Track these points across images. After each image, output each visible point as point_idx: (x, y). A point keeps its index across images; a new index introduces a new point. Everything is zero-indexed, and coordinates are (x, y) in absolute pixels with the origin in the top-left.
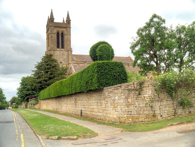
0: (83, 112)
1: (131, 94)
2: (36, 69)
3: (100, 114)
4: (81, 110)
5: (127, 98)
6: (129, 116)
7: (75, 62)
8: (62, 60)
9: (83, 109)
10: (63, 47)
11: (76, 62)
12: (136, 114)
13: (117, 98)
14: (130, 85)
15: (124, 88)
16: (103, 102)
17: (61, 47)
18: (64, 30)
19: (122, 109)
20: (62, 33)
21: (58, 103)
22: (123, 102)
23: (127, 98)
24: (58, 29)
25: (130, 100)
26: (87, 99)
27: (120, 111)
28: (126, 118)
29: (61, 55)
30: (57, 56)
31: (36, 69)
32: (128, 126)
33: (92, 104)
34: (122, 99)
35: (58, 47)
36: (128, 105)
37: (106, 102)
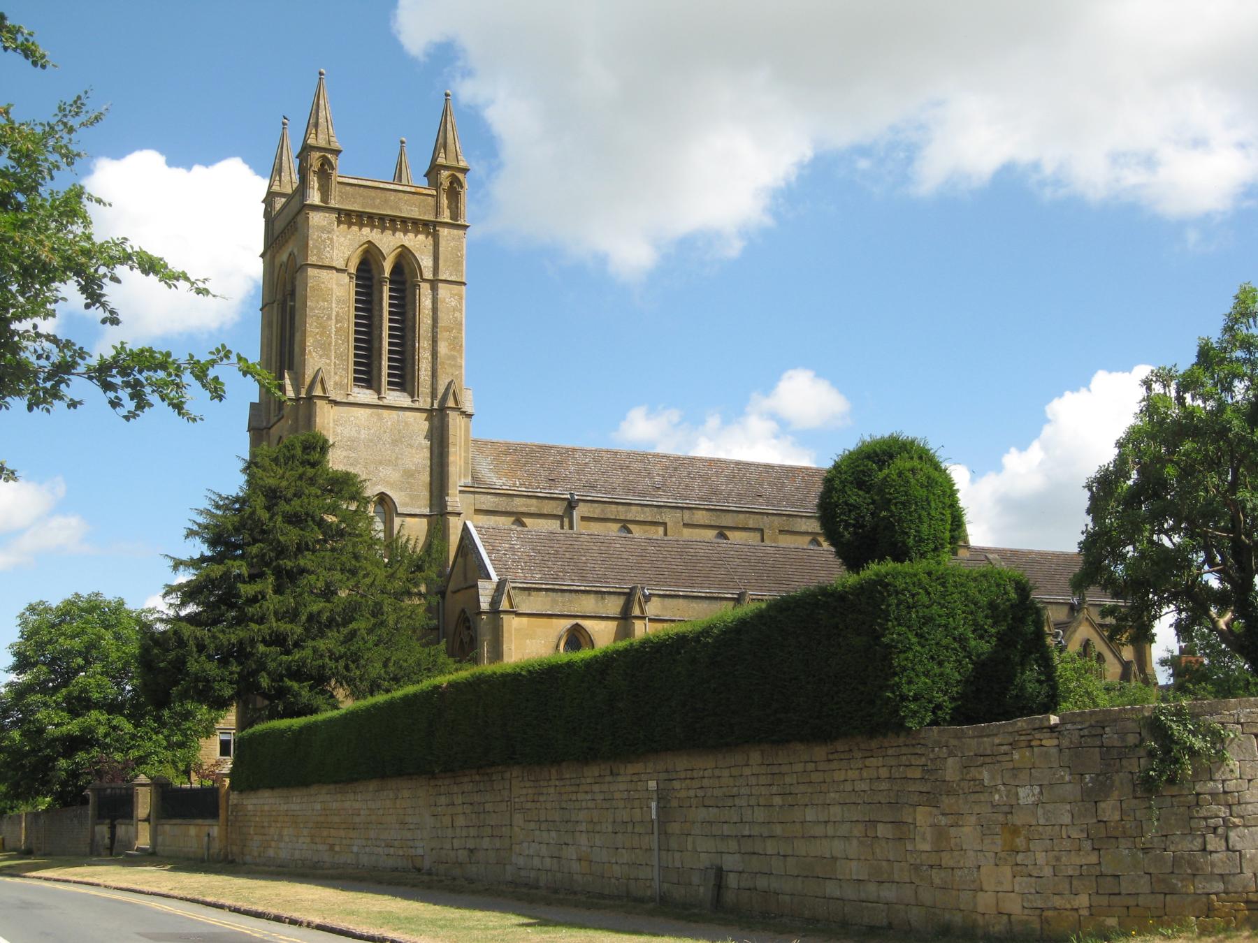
0: (732, 881)
1: (1116, 778)
2: (199, 548)
3: (889, 893)
4: (720, 873)
5: (1093, 796)
6: (1104, 901)
7: (488, 502)
8: (392, 485)
9: (730, 862)
10: (404, 379)
11: (502, 504)
12: (1147, 889)
13: (1027, 795)
14: (1115, 721)
15: (1075, 739)
16: (923, 816)
17: (385, 379)
18: (417, 243)
19: (1058, 859)
20: (398, 269)
21: (460, 821)
22: (1067, 819)
23: (1093, 796)
24: (368, 234)
25: (1109, 810)
26: (777, 800)
27: (1048, 871)
28: (1085, 912)
29: (386, 437)
30: (352, 444)
31: (199, 548)
32: (1248, 937)
33: (819, 830)
34: (1063, 801)
35: (366, 375)
36: (1102, 838)
37: (943, 821)
